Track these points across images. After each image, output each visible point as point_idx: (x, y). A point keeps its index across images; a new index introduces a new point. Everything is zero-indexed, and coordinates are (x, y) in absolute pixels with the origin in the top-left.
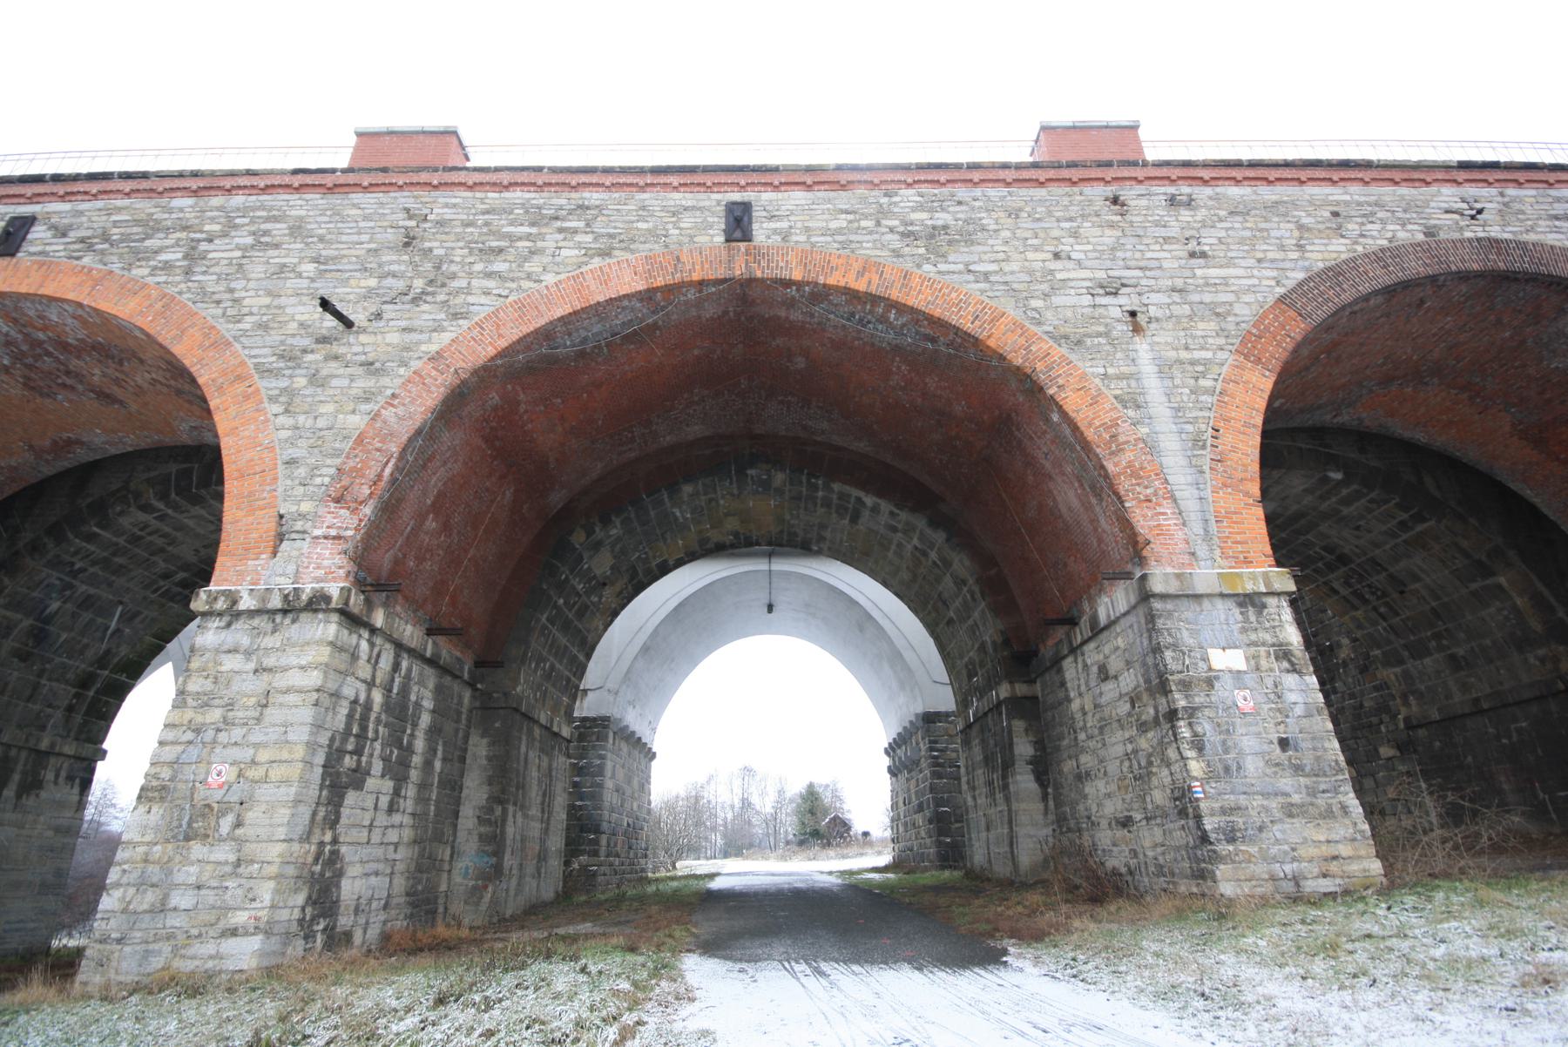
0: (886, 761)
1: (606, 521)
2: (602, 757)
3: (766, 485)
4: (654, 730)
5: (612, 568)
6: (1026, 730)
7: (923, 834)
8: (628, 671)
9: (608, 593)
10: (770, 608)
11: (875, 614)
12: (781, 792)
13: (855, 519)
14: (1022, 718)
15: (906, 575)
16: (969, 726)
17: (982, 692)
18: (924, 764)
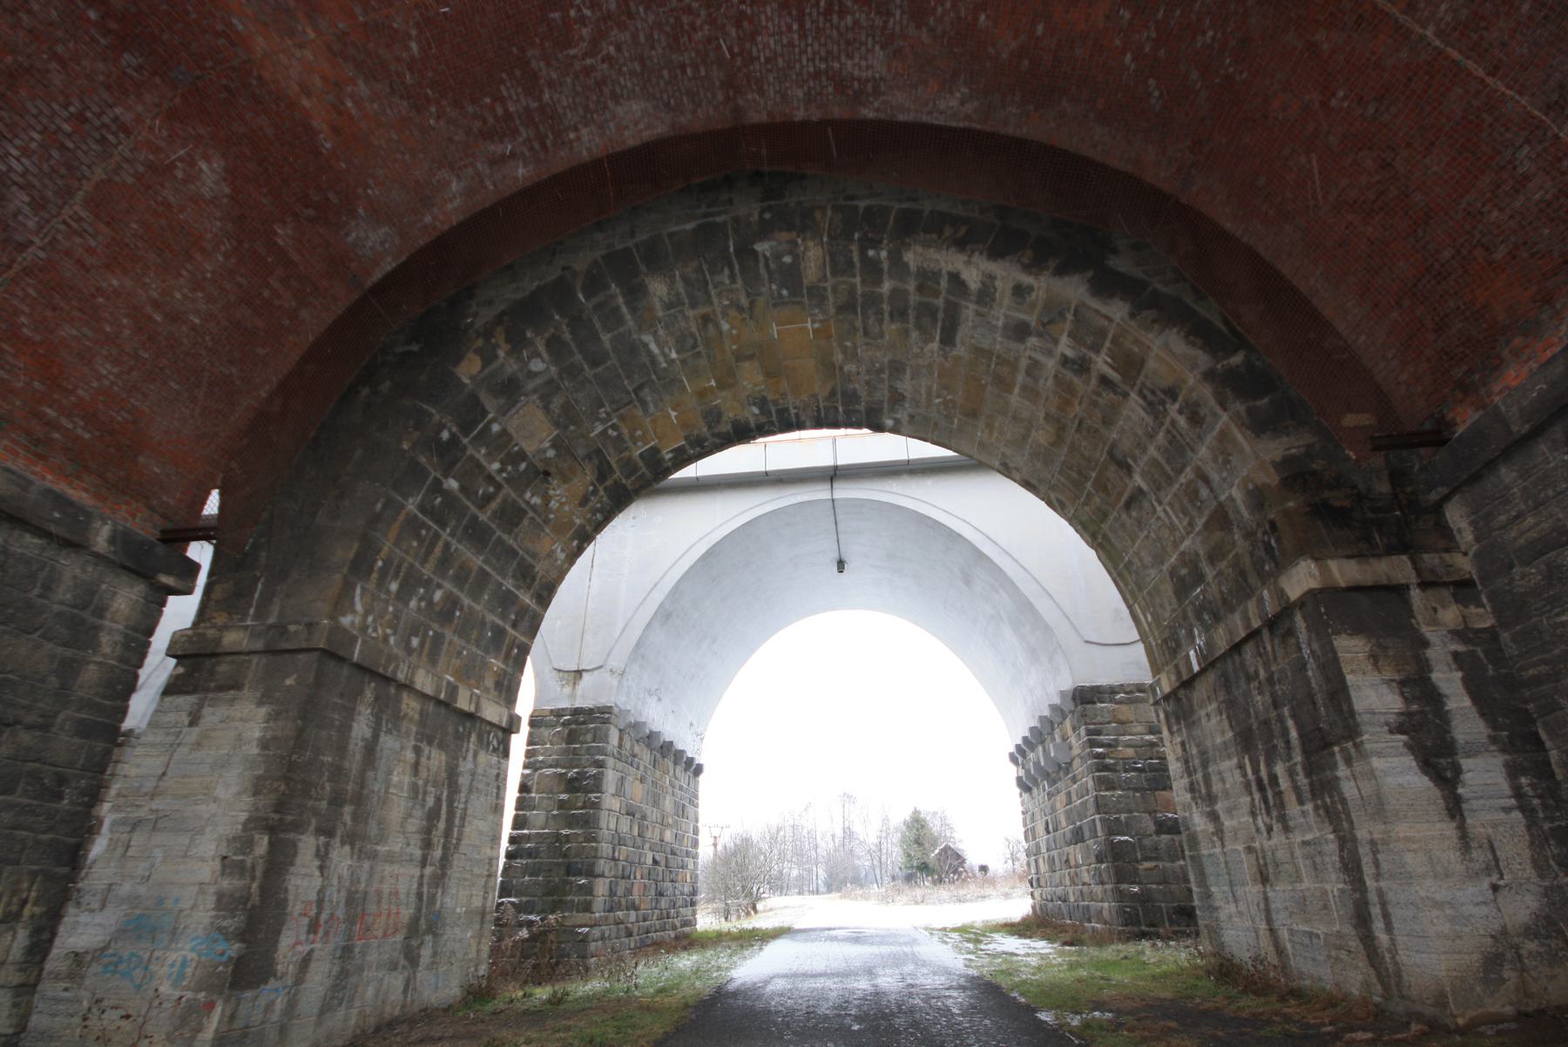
0: (1012, 772)
1: (517, 343)
2: (600, 765)
3: (791, 276)
4: (700, 737)
5: (555, 444)
6: (1374, 658)
7: (1086, 877)
8: (638, 645)
9: (560, 496)
10: (841, 565)
11: (987, 549)
12: (886, 820)
13: (948, 339)
14: (1356, 631)
15: (1042, 436)
16: (1188, 683)
17: (1213, 613)
18: (1079, 768)
